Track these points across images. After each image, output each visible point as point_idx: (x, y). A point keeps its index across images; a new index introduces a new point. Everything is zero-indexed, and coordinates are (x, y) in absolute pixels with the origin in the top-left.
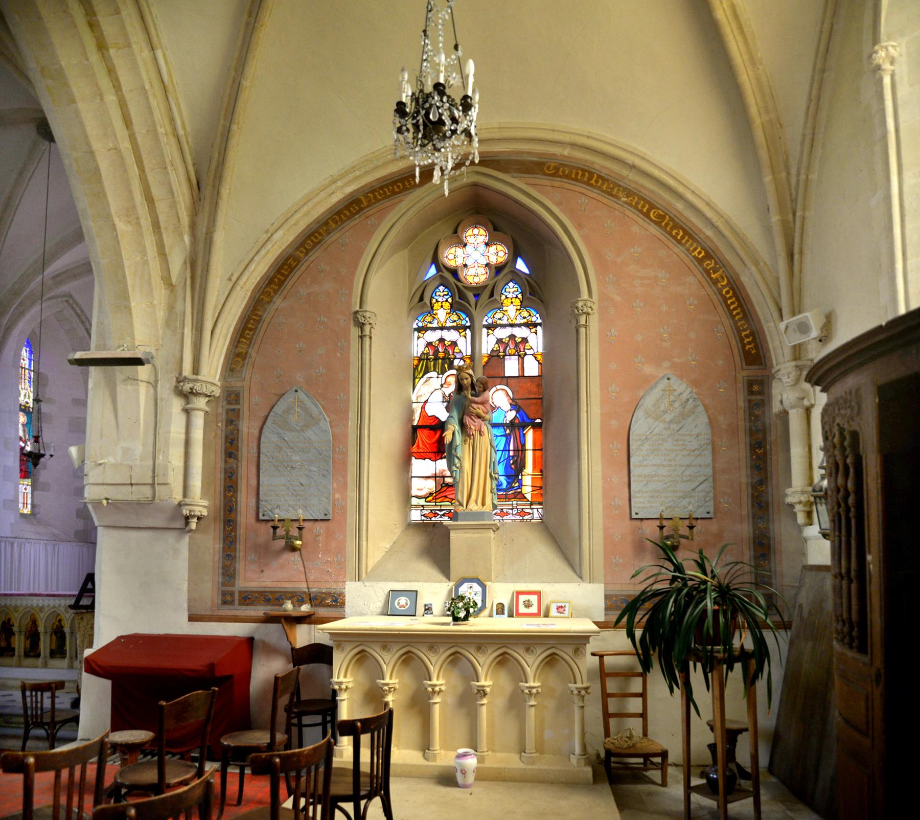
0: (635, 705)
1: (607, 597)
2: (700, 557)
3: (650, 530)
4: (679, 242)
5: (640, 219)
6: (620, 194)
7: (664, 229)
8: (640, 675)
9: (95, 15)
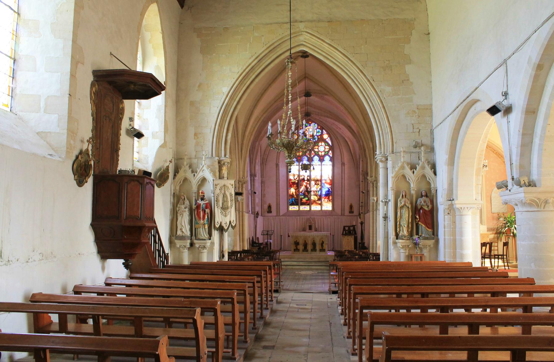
0: (496, 248)
1: (487, 228)
2: (257, 217)
3: (496, 215)
4: (500, 158)
5: (492, 153)
6: (488, 148)
7: (497, 155)
8: (497, 242)
9: (541, 135)
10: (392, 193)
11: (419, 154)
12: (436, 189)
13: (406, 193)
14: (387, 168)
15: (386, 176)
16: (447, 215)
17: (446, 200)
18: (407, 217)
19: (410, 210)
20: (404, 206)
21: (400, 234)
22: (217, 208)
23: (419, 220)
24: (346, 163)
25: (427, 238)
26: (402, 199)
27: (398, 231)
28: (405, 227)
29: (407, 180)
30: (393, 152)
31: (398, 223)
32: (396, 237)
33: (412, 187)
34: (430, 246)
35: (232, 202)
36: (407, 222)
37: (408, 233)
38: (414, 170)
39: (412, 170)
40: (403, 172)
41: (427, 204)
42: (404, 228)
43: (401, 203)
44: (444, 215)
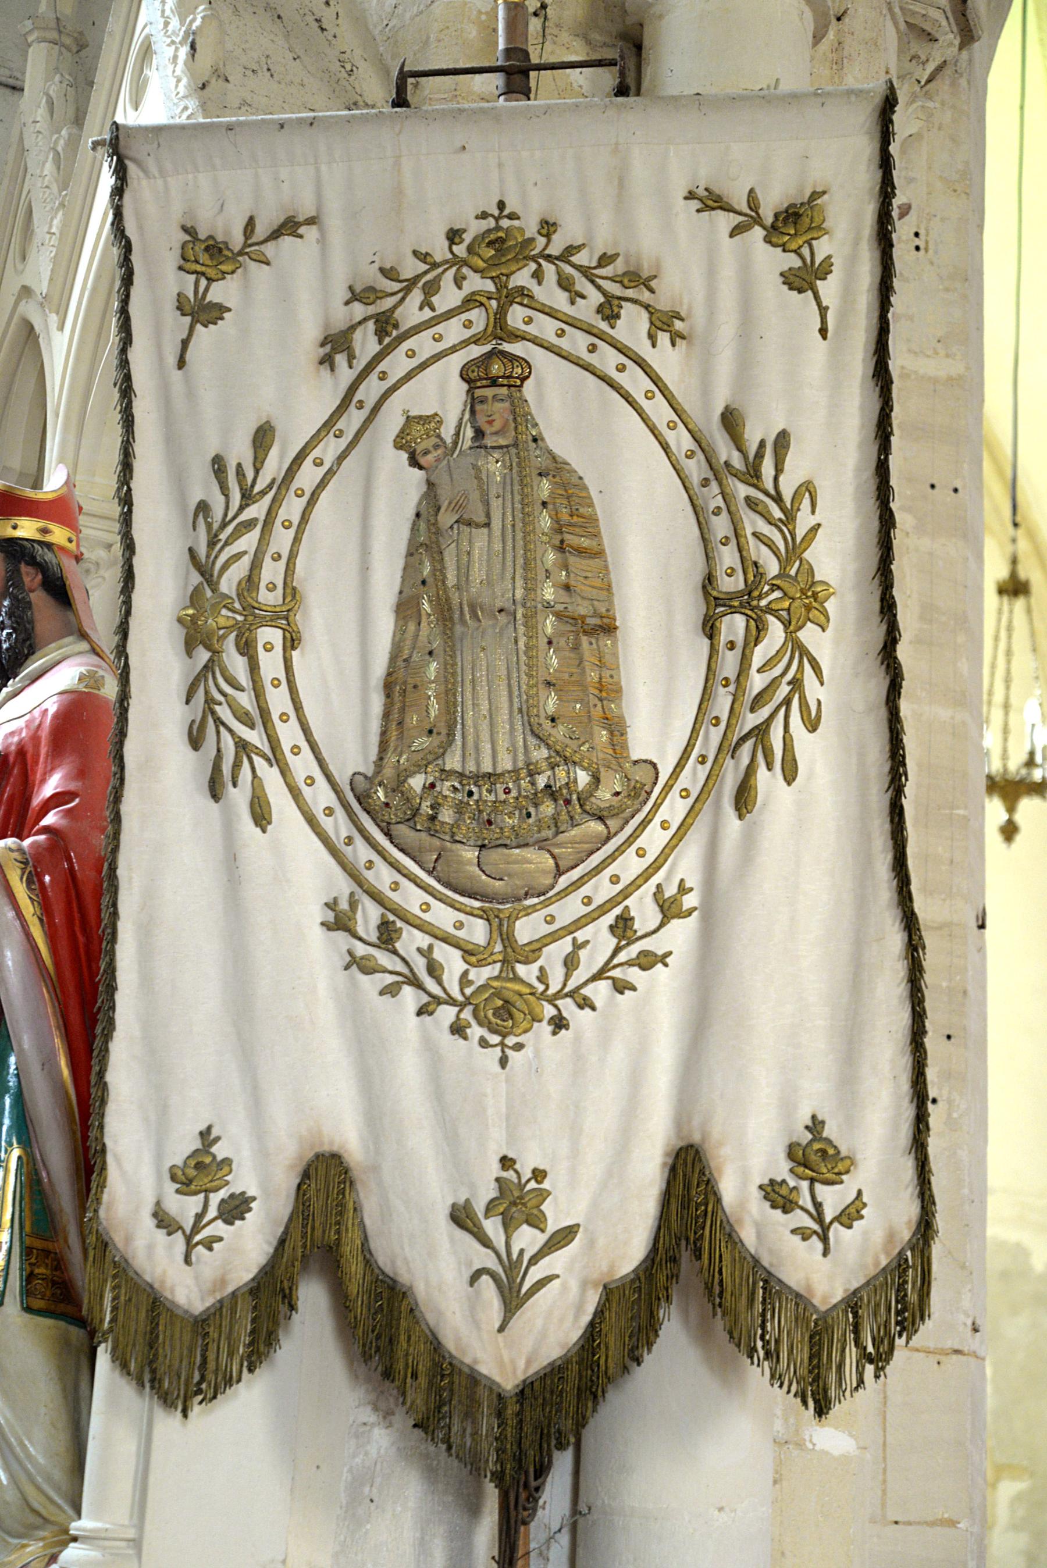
22: (215, 789)
35: (734, 626)
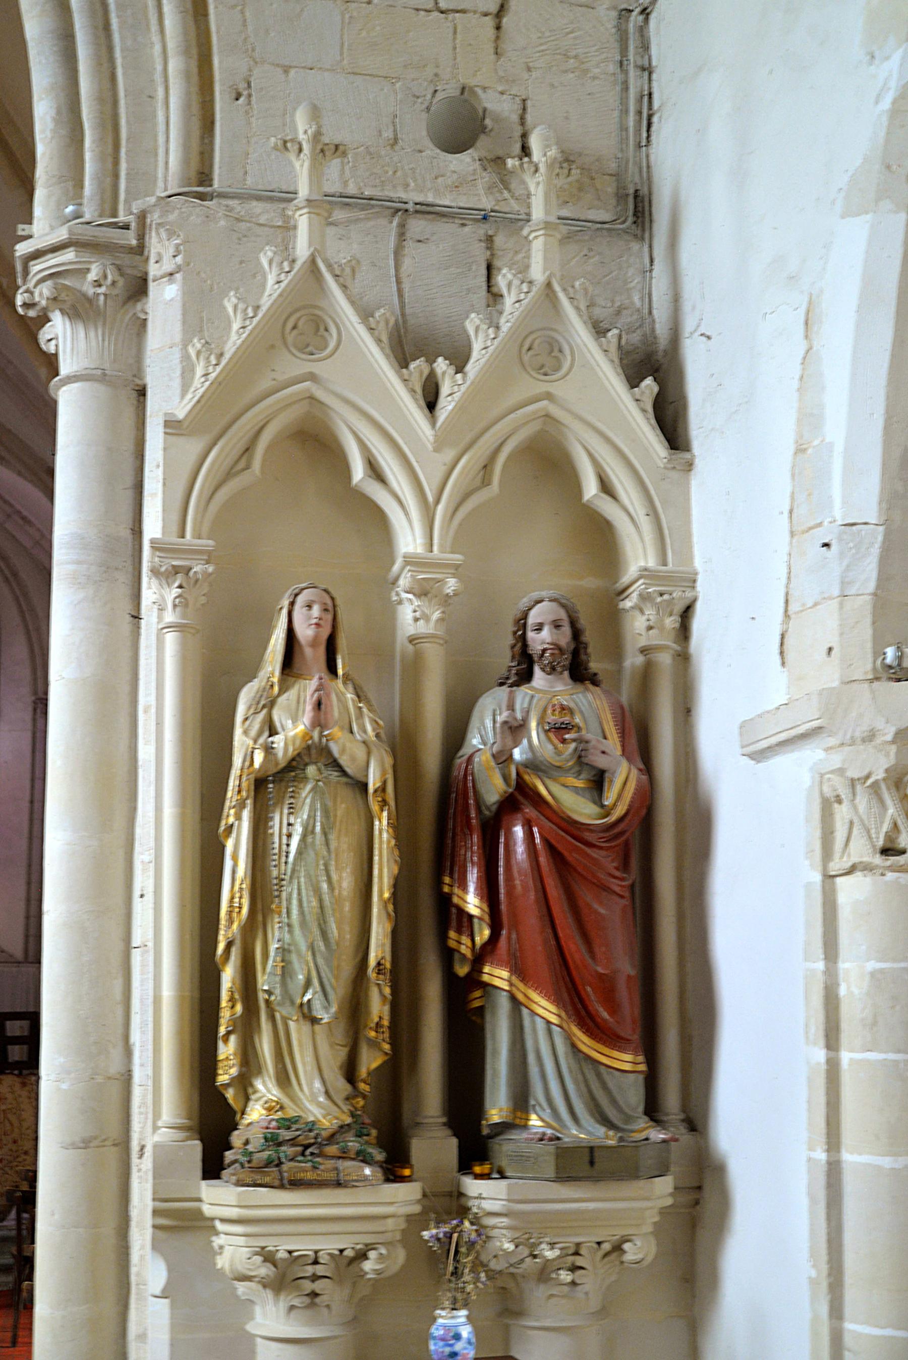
10: (170, 617)
11: (489, 240)
12: (679, 596)
13: (332, 610)
14: (142, 392)
15: (129, 446)
16: (867, 868)
17: (864, 667)
18: (338, 901)
19: (382, 824)
20: (311, 770)
21: (255, 1113)
23: (483, 934)
24: (284, 864)
25: (592, 1152)
26: (283, 690)
27: (223, 1078)
28: (314, 1021)
29: (358, 471)
30: (204, 177)
31: (228, 977)
32: (196, 1147)
33: (410, 561)
34: (618, 1248)
36: (347, 969)
37: (357, 1093)
38: (441, 365)
39: (418, 366)
40: (312, 377)
41: (580, 760)
42: (297, 1030)
43: (273, 732)
44: (829, 878)
